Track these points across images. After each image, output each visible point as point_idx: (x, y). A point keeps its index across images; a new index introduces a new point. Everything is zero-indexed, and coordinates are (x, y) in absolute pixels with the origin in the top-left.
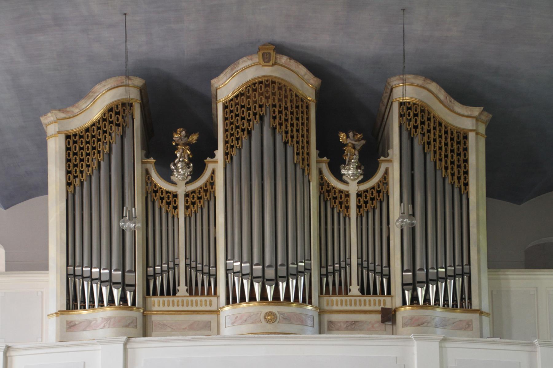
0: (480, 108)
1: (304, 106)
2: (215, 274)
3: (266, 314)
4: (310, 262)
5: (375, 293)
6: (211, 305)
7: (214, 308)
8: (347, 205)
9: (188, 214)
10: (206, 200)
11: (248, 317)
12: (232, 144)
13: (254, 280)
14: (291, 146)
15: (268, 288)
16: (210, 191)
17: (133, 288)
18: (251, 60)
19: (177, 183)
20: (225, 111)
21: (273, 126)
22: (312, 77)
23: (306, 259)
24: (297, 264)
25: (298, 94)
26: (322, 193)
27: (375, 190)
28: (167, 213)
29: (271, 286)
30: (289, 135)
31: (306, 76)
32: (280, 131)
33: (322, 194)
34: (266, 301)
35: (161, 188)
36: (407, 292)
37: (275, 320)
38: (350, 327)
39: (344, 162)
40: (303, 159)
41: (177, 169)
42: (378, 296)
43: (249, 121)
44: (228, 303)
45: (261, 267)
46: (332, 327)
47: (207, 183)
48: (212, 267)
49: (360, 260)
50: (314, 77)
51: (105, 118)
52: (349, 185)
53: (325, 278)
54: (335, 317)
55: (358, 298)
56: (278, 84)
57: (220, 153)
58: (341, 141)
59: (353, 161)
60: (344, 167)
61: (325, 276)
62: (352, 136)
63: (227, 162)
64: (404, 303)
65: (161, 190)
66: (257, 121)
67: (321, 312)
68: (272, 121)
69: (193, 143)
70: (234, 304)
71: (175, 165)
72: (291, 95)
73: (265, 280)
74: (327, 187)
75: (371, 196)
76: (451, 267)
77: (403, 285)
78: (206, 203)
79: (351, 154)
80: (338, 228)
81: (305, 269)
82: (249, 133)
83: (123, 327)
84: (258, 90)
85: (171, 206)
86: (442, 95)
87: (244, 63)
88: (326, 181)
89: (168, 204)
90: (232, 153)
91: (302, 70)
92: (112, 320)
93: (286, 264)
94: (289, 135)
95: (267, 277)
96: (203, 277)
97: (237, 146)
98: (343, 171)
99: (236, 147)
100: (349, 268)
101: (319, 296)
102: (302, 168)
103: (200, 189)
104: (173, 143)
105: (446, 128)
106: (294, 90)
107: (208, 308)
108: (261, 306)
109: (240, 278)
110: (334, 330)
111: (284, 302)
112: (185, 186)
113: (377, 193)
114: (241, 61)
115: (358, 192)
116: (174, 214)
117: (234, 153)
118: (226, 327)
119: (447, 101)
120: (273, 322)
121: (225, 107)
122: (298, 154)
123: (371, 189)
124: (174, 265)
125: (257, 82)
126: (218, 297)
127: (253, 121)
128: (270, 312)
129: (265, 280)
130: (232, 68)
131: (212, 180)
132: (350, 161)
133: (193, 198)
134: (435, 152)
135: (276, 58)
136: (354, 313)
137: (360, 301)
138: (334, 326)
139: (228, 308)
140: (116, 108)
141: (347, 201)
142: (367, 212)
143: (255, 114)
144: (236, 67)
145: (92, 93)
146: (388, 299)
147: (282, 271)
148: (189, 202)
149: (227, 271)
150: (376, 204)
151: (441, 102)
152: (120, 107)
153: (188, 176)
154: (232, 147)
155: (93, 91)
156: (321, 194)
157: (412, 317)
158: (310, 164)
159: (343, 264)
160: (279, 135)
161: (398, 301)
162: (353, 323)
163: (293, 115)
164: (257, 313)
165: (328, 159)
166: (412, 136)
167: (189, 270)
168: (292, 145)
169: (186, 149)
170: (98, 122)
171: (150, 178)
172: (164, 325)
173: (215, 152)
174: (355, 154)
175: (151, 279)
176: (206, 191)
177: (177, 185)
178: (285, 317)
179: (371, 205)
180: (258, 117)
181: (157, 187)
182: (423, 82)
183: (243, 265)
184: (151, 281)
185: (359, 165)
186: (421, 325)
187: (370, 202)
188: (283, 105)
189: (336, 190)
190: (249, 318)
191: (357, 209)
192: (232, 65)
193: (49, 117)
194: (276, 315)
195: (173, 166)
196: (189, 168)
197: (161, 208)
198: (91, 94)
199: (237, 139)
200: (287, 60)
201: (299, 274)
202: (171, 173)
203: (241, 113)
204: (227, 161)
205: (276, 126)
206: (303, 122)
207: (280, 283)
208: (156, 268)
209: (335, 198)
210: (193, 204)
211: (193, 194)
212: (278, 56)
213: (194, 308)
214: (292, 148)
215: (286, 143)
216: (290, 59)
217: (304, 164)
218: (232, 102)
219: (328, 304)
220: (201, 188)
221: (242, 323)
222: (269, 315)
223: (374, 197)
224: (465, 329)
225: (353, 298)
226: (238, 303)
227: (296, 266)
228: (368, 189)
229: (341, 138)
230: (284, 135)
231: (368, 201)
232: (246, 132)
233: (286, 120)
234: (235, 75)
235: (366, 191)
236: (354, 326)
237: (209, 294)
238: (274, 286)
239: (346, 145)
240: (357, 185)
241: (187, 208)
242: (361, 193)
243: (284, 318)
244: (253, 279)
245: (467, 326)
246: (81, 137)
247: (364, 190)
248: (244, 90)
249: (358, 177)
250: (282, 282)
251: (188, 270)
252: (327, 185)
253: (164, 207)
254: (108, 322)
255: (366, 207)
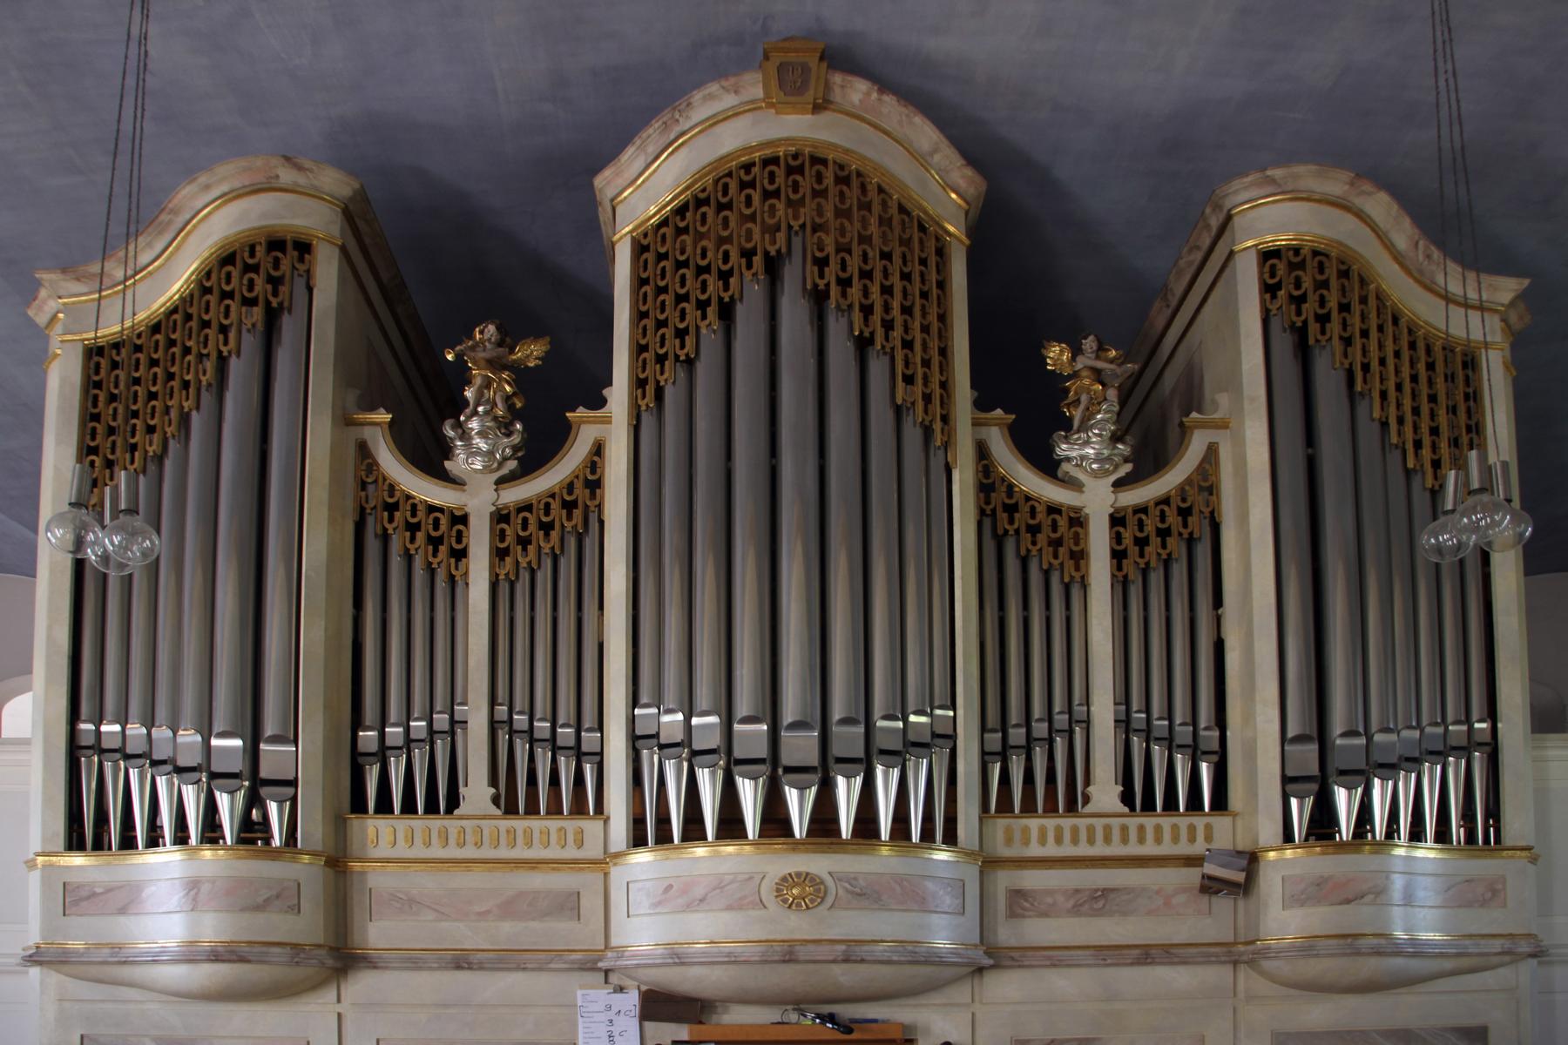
0: (1520, 280)
1: (931, 245)
2: (599, 750)
3: (784, 879)
4: (951, 713)
5: (1171, 804)
6: (580, 844)
7: (593, 850)
8: (1075, 548)
9: (503, 572)
10: (569, 532)
11: (714, 890)
12: (661, 352)
13: (736, 769)
14: (885, 353)
15: (792, 795)
16: (587, 507)
17: (290, 791)
18: (736, 92)
19: (467, 480)
20: (638, 261)
21: (816, 286)
22: (959, 164)
23: (936, 704)
24: (905, 719)
25: (909, 206)
26: (988, 512)
27: (1174, 506)
28: (431, 572)
29: (802, 789)
30: (877, 318)
31: (937, 158)
32: (841, 301)
33: (987, 515)
34: (782, 840)
35: (409, 497)
36: (1294, 802)
37: (819, 900)
38: (1087, 906)
39: (1066, 424)
40: (927, 398)
41: (465, 435)
42: (1208, 815)
43: (725, 276)
44: (638, 840)
45: (765, 727)
46: (1024, 909)
47: (576, 480)
48: (590, 730)
49: (1123, 708)
50: (962, 165)
51: (208, 284)
52: (1084, 489)
53: (999, 764)
54: (1032, 879)
55: (1116, 823)
56: (837, 168)
57: (619, 394)
58: (1049, 368)
59: (1099, 416)
60: (1066, 437)
61: (998, 758)
62: (1095, 348)
63: (643, 408)
64: (1288, 837)
65: (411, 501)
66: (755, 275)
67: (989, 863)
68: (812, 272)
69: (527, 367)
70: (659, 847)
71: (459, 425)
72: (884, 204)
73: (780, 771)
74: (1004, 495)
75: (1160, 525)
76: (1436, 724)
77: (1286, 780)
78: (572, 543)
79: (1092, 399)
80: (1021, 620)
81: (935, 735)
82: (727, 313)
83: (243, 910)
84: (762, 182)
85: (443, 549)
86: (1403, 234)
87: (708, 102)
88: (1003, 479)
89: (435, 542)
90: (662, 379)
91: (925, 134)
92: (205, 888)
93: (862, 718)
94: (877, 318)
95: (787, 758)
96: (554, 760)
97: (679, 352)
98: (1063, 449)
99: (677, 357)
100: (1081, 733)
101: (981, 819)
102: (921, 423)
103: (550, 500)
104: (450, 353)
105: (1410, 331)
106: (892, 191)
107: (571, 852)
108: (765, 853)
109: (685, 764)
110: (1030, 917)
111: (855, 841)
112: (496, 490)
113: (1179, 515)
114: (697, 96)
115: (1117, 510)
116: (454, 572)
117: (666, 375)
118: (628, 917)
119: (1417, 256)
120: (811, 906)
121: (639, 249)
122: (909, 380)
123: (1157, 504)
124: (453, 722)
125: (757, 160)
126: (606, 821)
127: (741, 274)
128: (799, 875)
129: (780, 771)
130: (665, 123)
131: (593, 472)
132: (1088, 416)
133: (525, 525)
134: (1384, 395)
135: (828, 87)
136: (1104, 864)
137: (1124, 829)
138: (1032, 905)
139: (643, 857)
140: (246, 255)
141: (1077, 538)
142: (1145, 572)
143: (748, 255)
144: (681, 120)
145: (169, 214)
146: (1221, 823)
147: (848, 740)
148: (508, 539)
149: (635, 741)
150: (1175, 545)
151: (1398, 257)
152: (260, 251)
153: (505, 459)
154: (661, 359)
155: (170, 206)
156: (984, 515)
157: (1322, 877)
158: (952, 416)
159: (1061, 720)
160: (837, 320)
161: (1269, 830)
162: (1100, 893)
163: (888, 263)
164: (747, 876)
165: (1006, 412)
166: (1023, 552)
167: (504, 737)
168: (888, 350)
169: (501, 379)
170: (188, 299)
171: (375, 468)
172: (412, 901)
173: (605, 392)
174: (1105, 399)
175: (371, 765)
176: (569, 506)
177: (466, 487)
178: (858, 890)
179: (1139, 560)
180: (758, 260)
181: (398, 494)
182: (1347, 187)
183: (695, 721)
184: (371, 769)
185: (1119, 433)
186: (1356, 899)
187: (1155, 541)
188: (853, 229)
189: (1036, 504)
190: (718, 891)
191: (1111, 562)
192: (666, 112)
193: (44, 302)
194: (822, 882)
195: (453, 428)
196: (508, 435)
197: (408, 558)
198: (164, 217)
199: (681, 334)
200: (868, 94)
201: (911, 749)
202: (447, 451)
203: (695, 254)
204: (642, 403)
205: (828, 285)
206: (926, 288)
207: (841, 781)
208: (387, 730)
209: (1034, 530)
210: (524, 542)
211: (522, 515)
212: (837, 78)
213: (520, 852)
214: (886, 359)
215: (863, 345)
216: (881, 91)
217: (930, 412)
218: (663, 230)
219: (1009, 841)
220: (553, 496)
221: (688, 906)
222: (795, 885)
223: (1169, 527)
224: (1484, 903)
225: (1099, 823)
226: (676, 841)
227: (900, 724)
228: (1148, 501)
229: (1049, 361)
230: (857, 316)
231: (1147, 537)
232: (712, 312)
233: (866, 275)
234: (682, 144)
235: (1142, 510)
236: (1100, 904)
237: (579, 808)
238: (814, 789)
239: (1075, 375)
240: (1112, 489)
241: (499, 554)
242: (1123, 514)
243: (852, 893)
244: (731, 767)
245: (1489, 895)
246: (138, 349)
247: (1135, 506)
248: (710, 188)
249: (1116, 467)
250: (848, 777)
251: (503, 738)
252: (1004, 489)
253: (419, 551)
254: (193, 893)
255: (1142, 555)
